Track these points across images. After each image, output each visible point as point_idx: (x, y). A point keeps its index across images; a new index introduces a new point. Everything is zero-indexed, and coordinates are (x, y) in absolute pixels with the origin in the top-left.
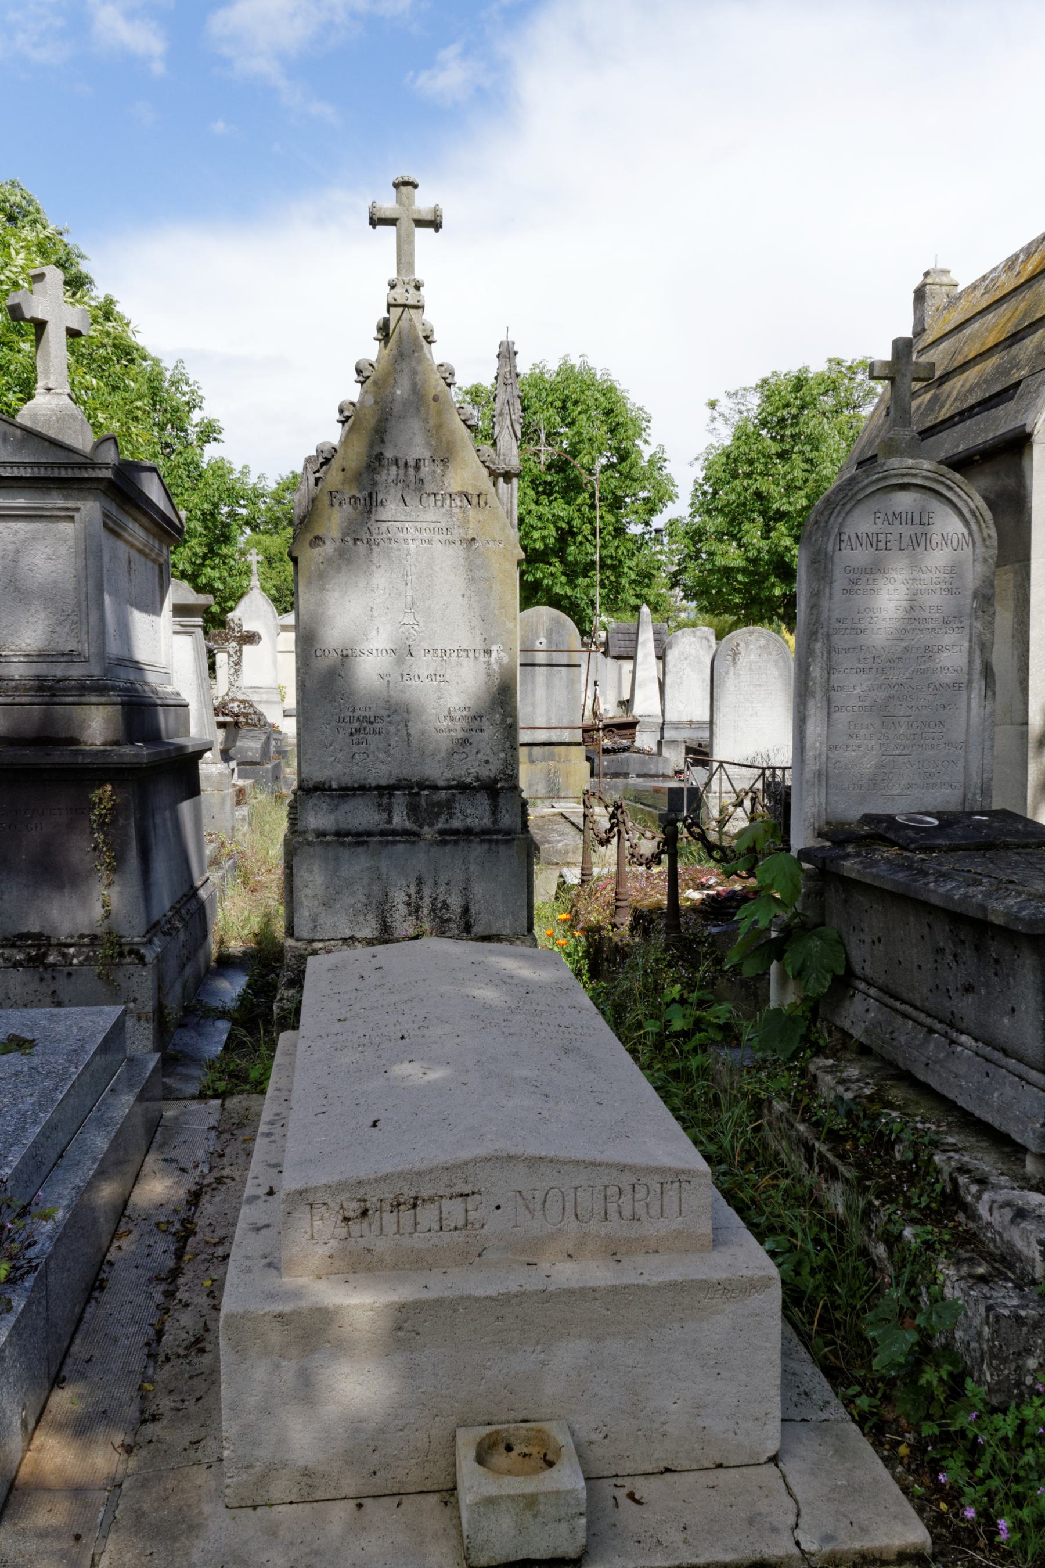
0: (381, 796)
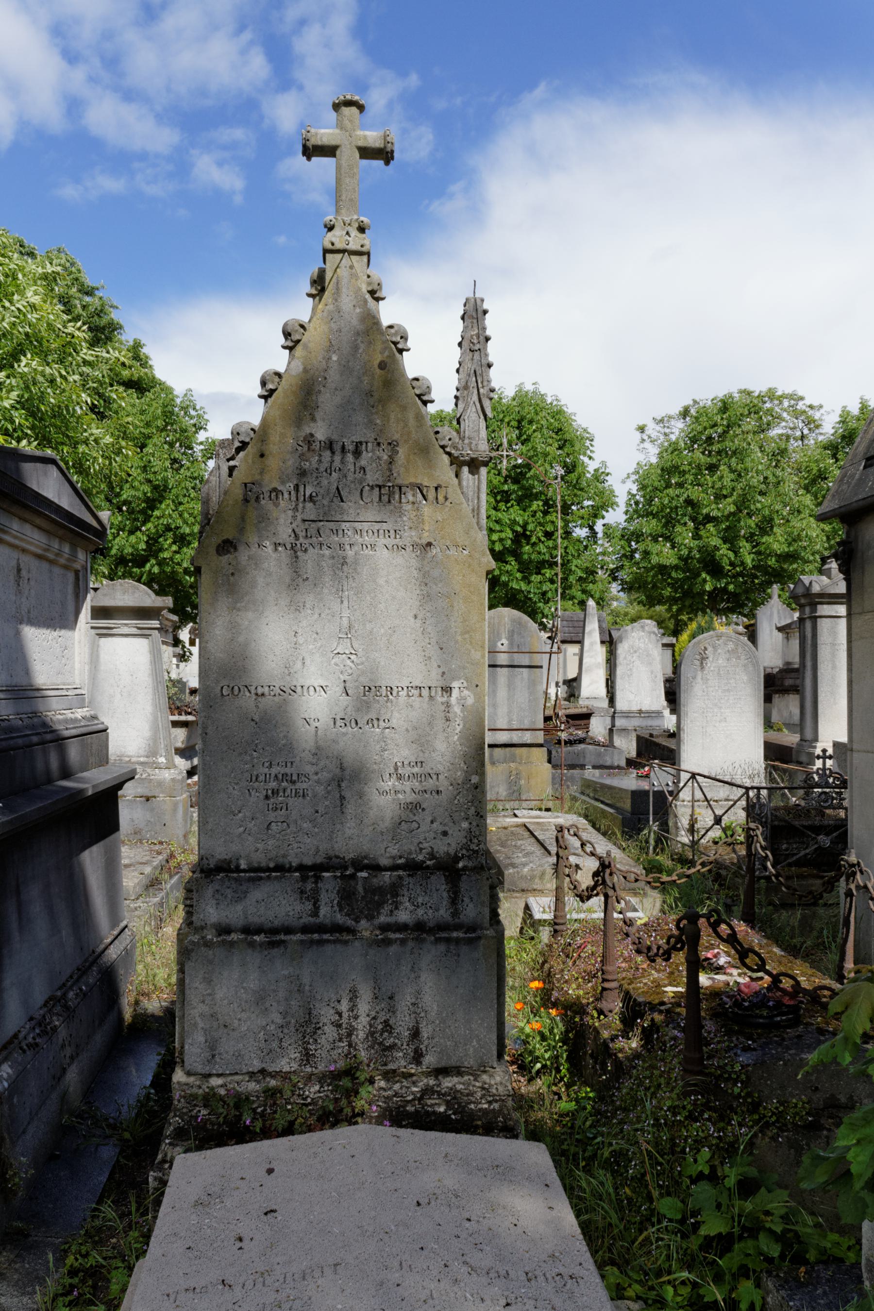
0: (304, 879)
